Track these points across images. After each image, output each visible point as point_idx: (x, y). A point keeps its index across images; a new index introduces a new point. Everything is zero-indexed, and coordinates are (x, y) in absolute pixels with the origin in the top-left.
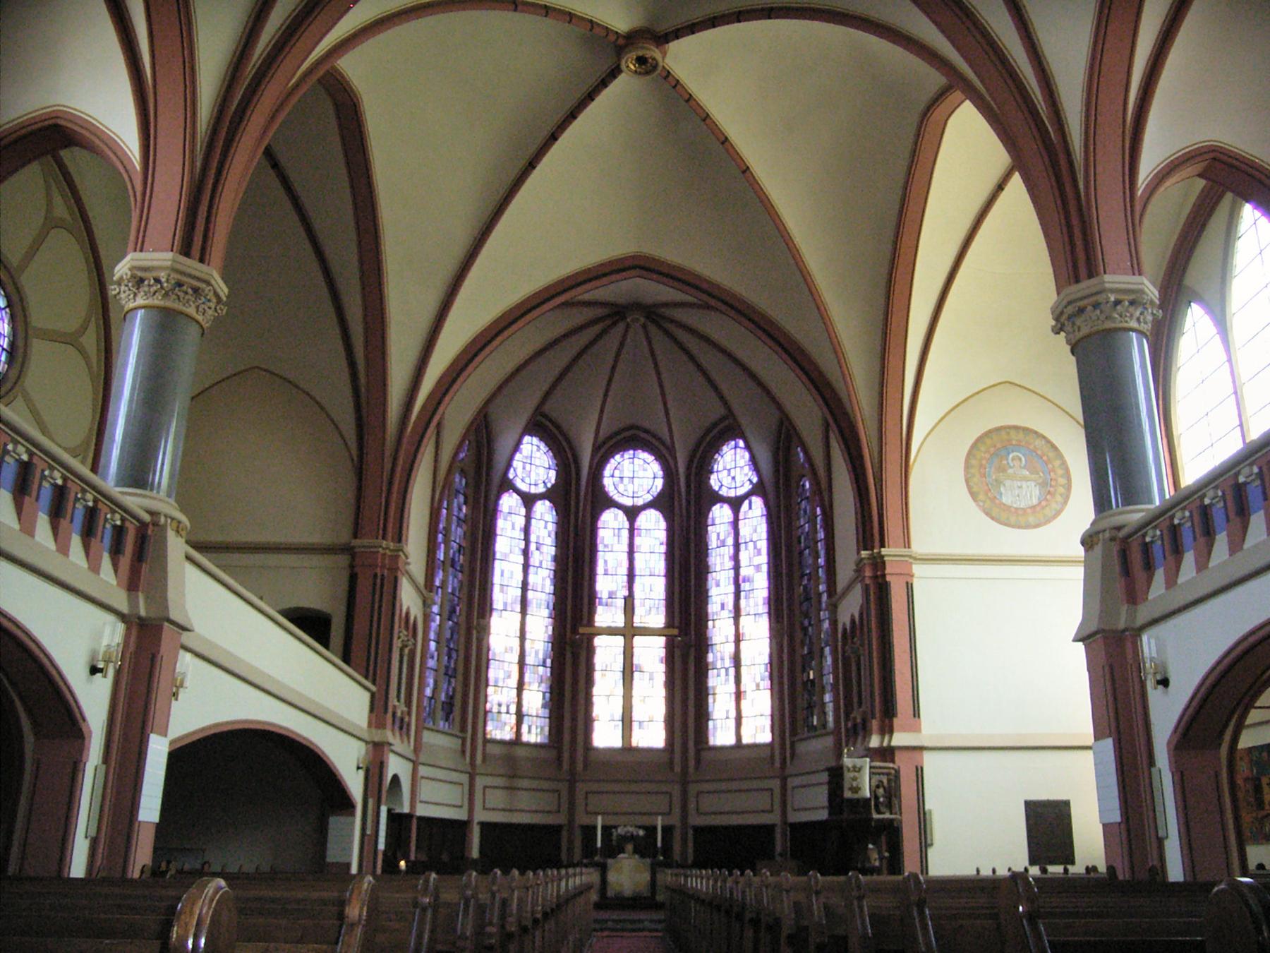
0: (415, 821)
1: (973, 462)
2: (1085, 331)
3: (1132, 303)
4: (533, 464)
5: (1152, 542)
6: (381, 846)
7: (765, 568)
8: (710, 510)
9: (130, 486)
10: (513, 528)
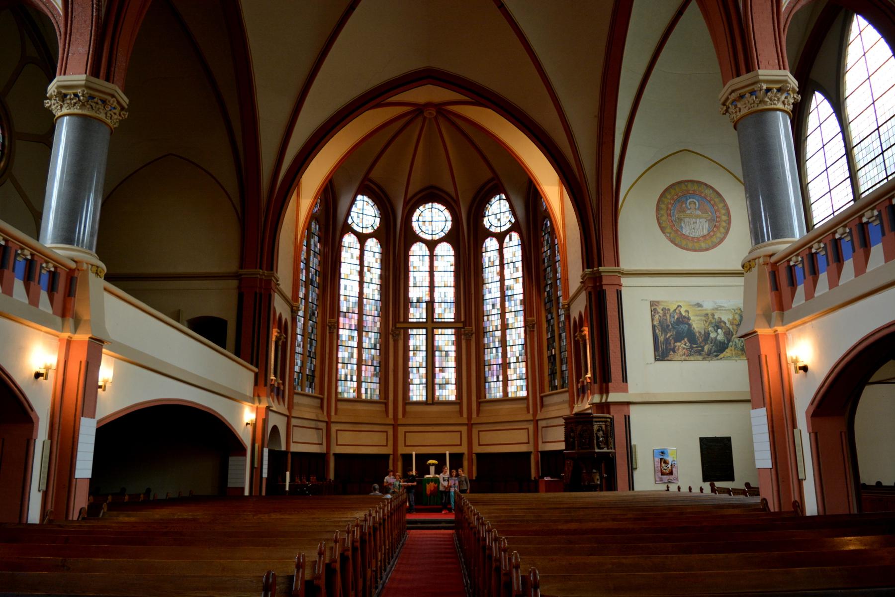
0: (290, 455)
1: (663, 206)
2: (744, 111)
3: (779, 90)
4: (364, 214)
5: (794, 266)
6: (265, 475)
7: (521, 280)
8: (484, 241)
9: (61, 243)
10: (352, 257)
